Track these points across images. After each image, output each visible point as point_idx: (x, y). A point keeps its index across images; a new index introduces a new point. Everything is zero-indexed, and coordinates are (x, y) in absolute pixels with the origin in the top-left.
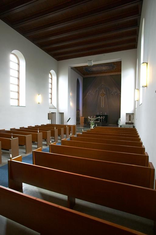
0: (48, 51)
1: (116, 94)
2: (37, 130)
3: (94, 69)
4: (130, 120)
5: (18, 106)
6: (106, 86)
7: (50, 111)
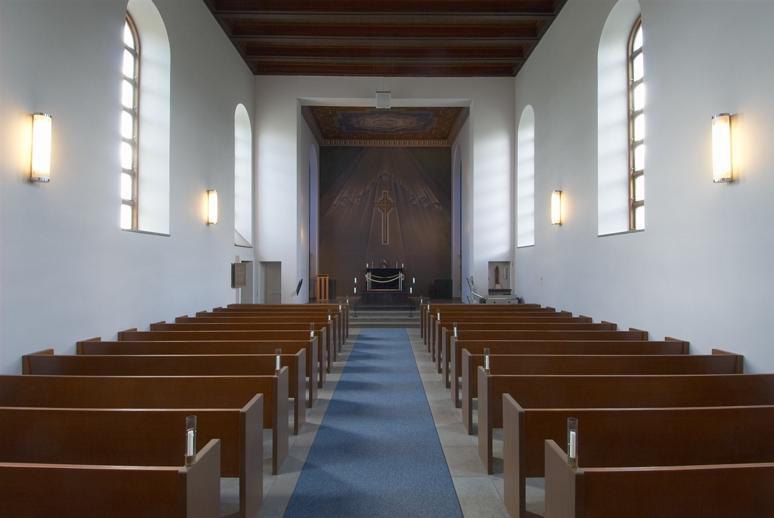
1: (426, 205)
2: (308, 327)
3: (370, 122)
4: (497, 282)
5: (135, 230)
7: (237, 257)
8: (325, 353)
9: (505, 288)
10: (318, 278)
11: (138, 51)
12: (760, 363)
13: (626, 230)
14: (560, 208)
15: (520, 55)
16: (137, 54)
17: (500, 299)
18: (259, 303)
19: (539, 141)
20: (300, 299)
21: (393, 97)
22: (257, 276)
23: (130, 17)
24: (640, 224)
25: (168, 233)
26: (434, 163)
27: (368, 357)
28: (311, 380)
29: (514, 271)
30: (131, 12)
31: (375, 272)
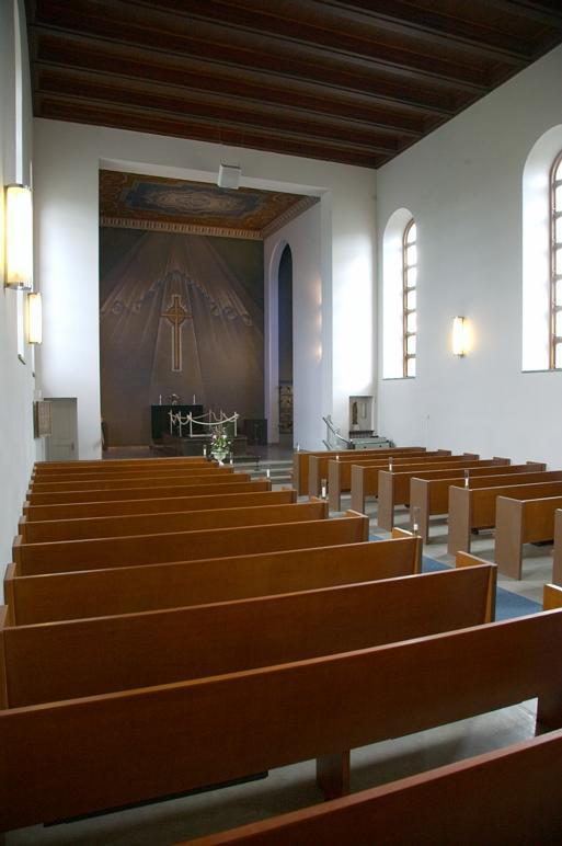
1: (231, 318)
2: (462, 474)
3: (172, 199)
6: (192, 282)
9: (364, 428)
12: (555, 465)
13: (547, 368)
15: (396, 146)
17: (362, 444)
24: (412, 373)
28: (433, 332)
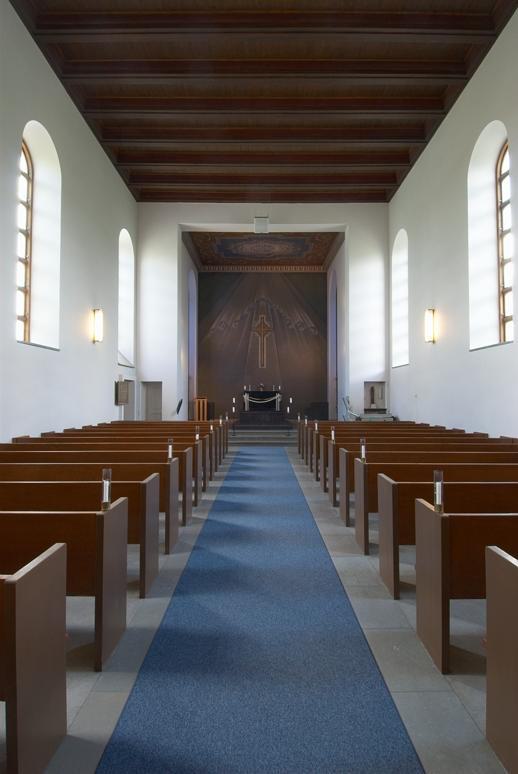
0: (120, 159)
3: (247, 248)
4: (373, 402)
5: (27, 342)
7: (120, 376)
8: (200, 473)
9: (381, 407)
10: (197, 401)
11: (31, 176)
14: (434, 326)
15: (393, 181)
16: (30, 178)
18: (140, 420)
19: (413, 263)
20: (182, 417)
21: (271, 222)
22: (138, 395)
23: (26, 146)
25: (58, 348)
26: (309, 283)
27: (239, 509)
29: (389, 393)
30: (26, 140)
31: (252, 394)
